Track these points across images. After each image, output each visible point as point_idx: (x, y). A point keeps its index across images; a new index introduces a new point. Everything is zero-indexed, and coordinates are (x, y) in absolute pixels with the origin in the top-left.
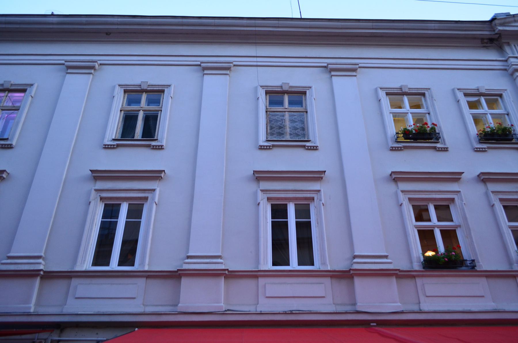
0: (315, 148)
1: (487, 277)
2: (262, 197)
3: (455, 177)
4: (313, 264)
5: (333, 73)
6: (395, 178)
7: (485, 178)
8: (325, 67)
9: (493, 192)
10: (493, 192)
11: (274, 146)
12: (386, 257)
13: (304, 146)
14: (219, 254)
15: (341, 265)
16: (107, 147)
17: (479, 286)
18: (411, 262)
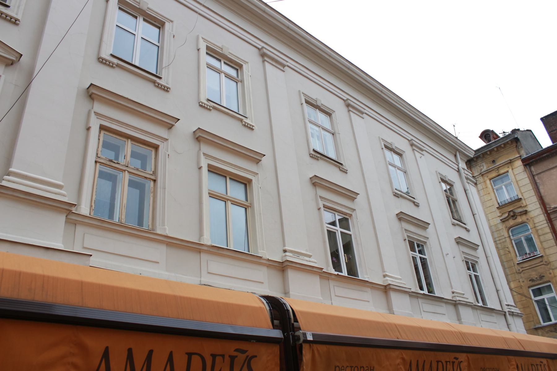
0: (166, 89)
1: (169, 244)
3: (168, 122)
4: (550, 320)
5: (266, 59)
6: (200, 136)
7: (201, 137)
8: (259, 49)
9: (204, 154)
10: (204, 154)
12: (310, 256)
13: (154, 82)
15: (278, 257)
16: (102, 61)
17: (158, 252)
18: (201, 234)
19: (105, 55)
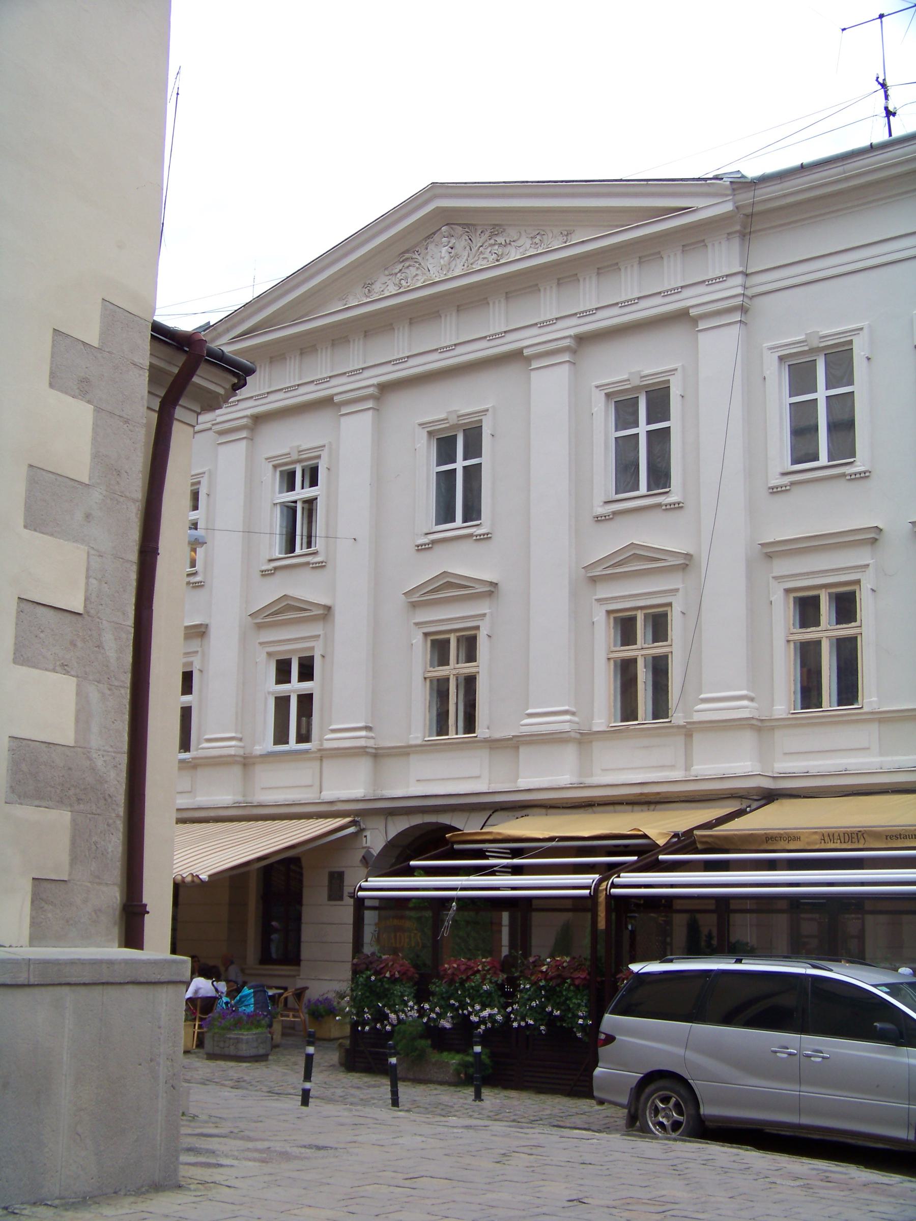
2: (261, 656)
11: (434, 542)
14: (573, 709)
19: (601, 510)
